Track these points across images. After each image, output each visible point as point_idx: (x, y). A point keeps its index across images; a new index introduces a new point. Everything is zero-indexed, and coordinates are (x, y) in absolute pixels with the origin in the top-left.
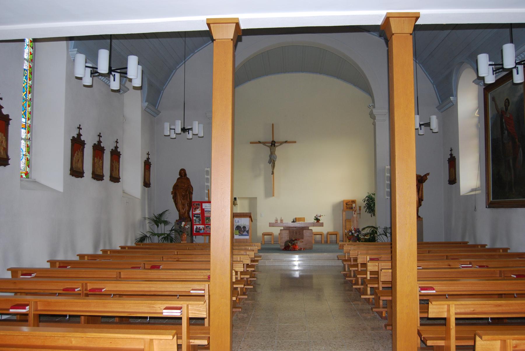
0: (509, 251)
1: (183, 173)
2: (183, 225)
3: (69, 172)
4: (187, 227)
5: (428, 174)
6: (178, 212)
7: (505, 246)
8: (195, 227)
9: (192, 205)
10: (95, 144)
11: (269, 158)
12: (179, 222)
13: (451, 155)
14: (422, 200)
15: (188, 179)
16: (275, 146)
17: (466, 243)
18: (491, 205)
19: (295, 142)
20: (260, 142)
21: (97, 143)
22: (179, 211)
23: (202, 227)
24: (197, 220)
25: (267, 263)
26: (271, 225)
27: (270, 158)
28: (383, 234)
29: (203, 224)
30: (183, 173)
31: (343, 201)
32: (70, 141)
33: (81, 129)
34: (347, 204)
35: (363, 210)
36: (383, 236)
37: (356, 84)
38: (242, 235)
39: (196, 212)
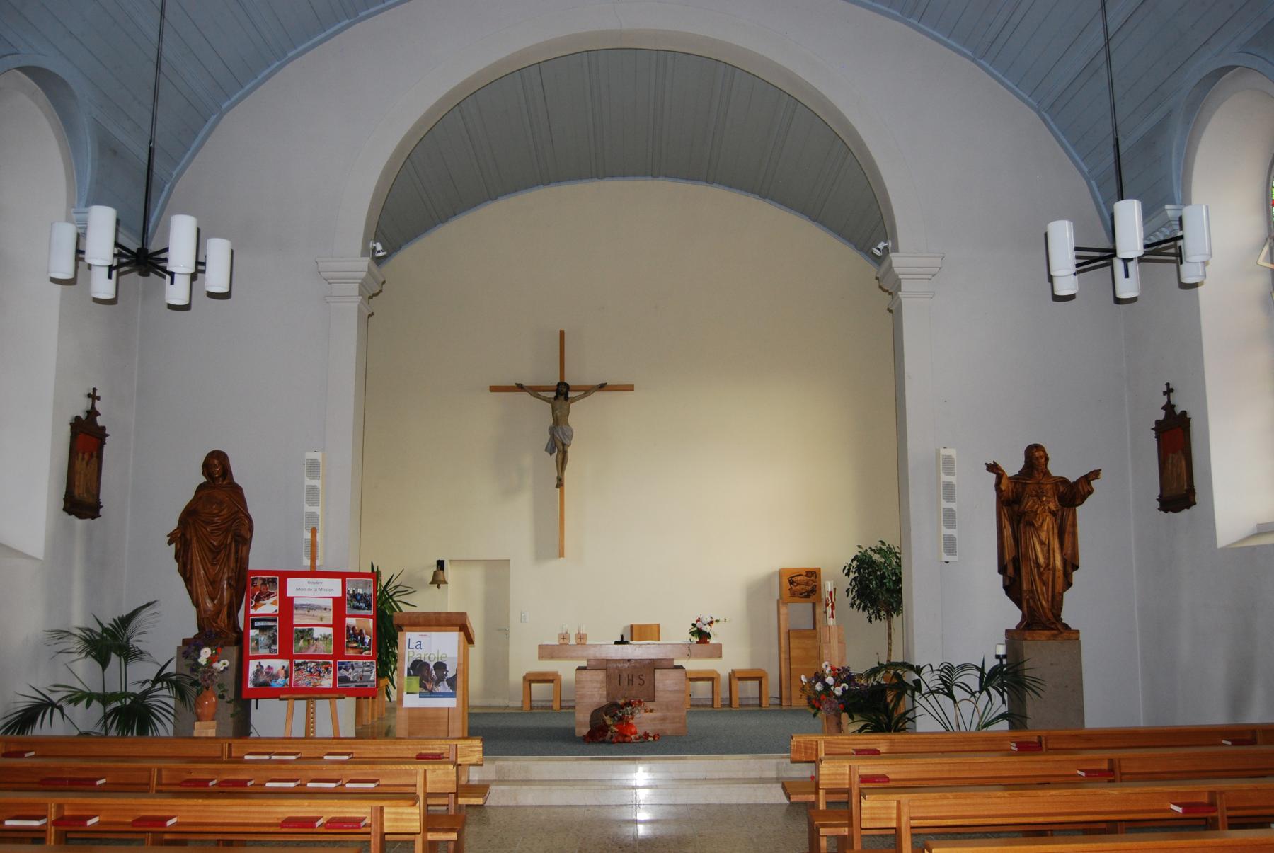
1: (217, 466)
2: (203, 660)
3: (62, 504)
4: (219, 666)
5: (1095, 474)
6: (194, 610)
8: (253, 666)
9: (245, 588)
10: (77, 418)
11: (548, 436)
12: (190, 648)
13: (1169, 407)
14: (1076, 567)
15: (237, 491)
16: (566, 398)
19: (630, 388)
20: (520, 388)
21: (83, 416)
22: (196, 603)
23: (278, 665)
24: (263, 639)
25: (529, 797)
26: (546, 652)
27: (553, 437)
28: (938, 691)
29: (285, 653)
30: (217, 466)
31: (781, 573)
32: (68, 428)
33: (98, 398)
34: (791, 582)
35: (844, 601)
36: (941, 698)
37: (814, 209)
38: (432, 694)
39: (260, 611)
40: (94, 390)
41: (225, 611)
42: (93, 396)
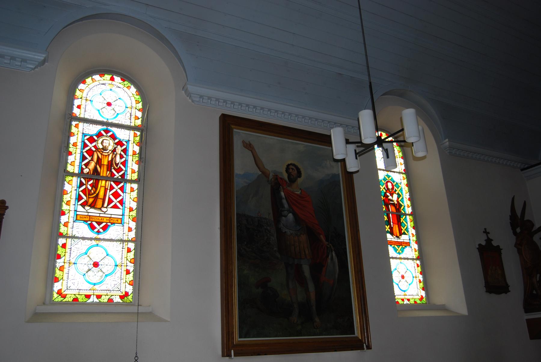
21: (484, 243)
33: (489, 233)
40: (485, 229)
41: (306, 270)
42: (486, 232)
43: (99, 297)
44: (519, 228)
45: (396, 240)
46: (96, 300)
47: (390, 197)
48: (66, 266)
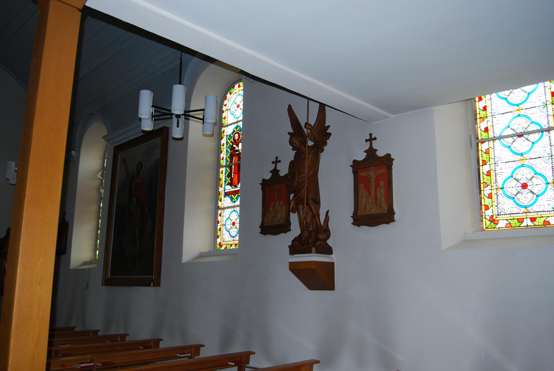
0: (128, 339)
7: (121, 332)
17: (73, 328)
18: (107, 282)
43: (533, 220)
44: (313, 143)
45: (234, 190)
46: (530, 223)
47: (237, 148)
48: (494, 192)
